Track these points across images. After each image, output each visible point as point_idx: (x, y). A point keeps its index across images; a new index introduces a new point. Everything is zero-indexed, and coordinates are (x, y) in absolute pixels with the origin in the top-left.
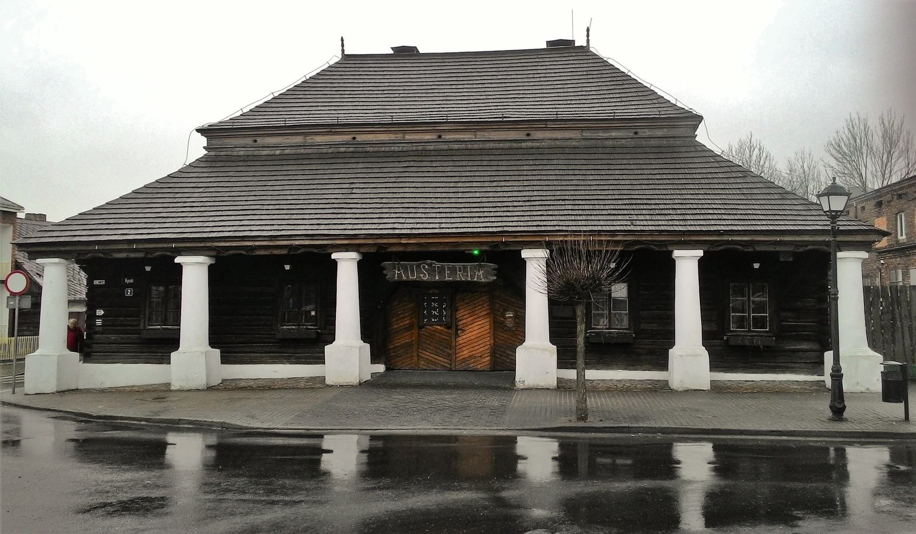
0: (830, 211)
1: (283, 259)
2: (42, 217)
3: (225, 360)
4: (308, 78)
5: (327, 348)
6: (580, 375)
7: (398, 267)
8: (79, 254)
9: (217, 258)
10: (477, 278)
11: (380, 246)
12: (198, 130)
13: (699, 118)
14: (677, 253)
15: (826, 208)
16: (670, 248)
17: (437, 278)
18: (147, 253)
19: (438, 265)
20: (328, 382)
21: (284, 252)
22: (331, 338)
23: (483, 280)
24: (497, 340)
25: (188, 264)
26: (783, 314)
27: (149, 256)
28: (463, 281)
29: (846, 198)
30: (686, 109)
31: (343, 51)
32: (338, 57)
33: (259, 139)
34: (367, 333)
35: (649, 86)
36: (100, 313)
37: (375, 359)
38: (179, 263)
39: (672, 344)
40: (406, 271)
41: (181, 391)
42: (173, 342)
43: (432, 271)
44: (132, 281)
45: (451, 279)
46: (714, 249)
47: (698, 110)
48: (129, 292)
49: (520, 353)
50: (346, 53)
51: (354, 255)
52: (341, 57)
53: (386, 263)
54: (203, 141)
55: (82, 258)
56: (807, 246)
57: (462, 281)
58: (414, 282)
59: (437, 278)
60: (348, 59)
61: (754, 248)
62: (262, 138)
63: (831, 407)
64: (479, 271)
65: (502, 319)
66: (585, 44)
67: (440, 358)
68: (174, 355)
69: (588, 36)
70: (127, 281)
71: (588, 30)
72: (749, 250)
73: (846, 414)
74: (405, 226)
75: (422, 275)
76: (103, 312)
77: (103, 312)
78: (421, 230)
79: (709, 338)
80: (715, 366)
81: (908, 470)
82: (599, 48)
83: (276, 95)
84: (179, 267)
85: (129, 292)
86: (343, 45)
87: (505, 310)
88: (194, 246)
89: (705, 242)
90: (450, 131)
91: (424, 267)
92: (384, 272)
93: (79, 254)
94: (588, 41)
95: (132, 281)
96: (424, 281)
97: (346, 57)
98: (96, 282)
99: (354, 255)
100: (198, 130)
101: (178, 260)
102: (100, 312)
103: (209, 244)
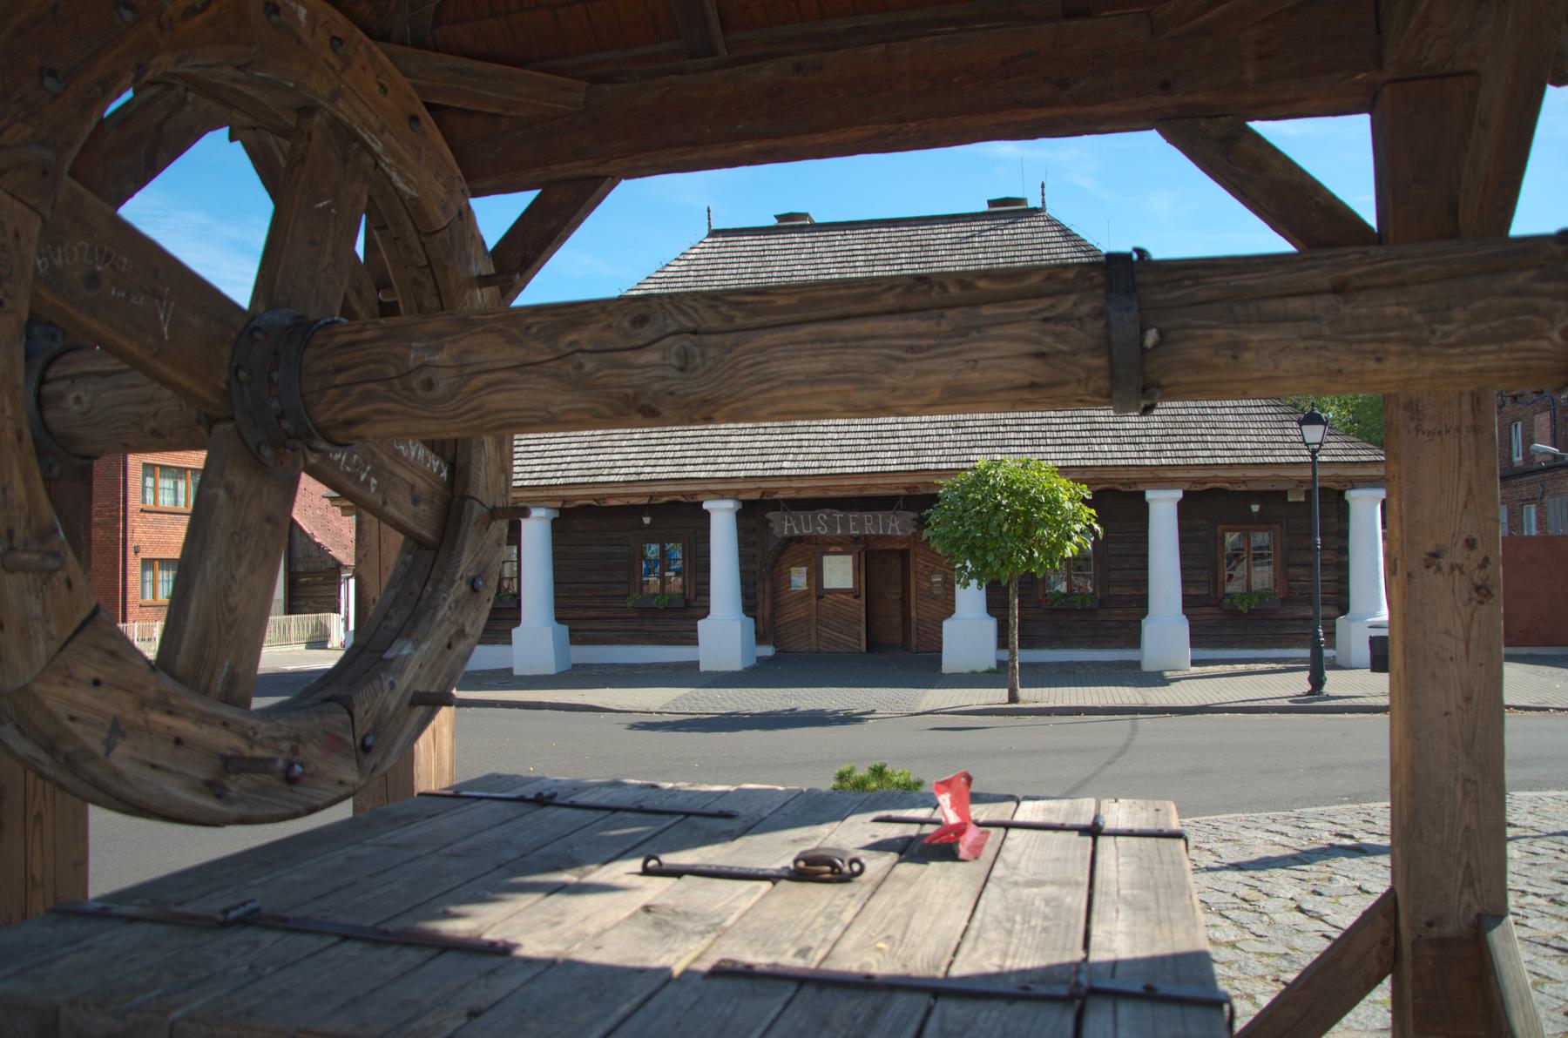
1: (639, 510)
3: (574, 641)
5: (701, 624)
7: (789, 519)
11: (765, 492)
14: (1150, 495)
17: (839, 532)
18: (564, 502)
19: (838, 515)
20: (516, 672)
22: (705, 611)
23: (899, 533)
24: (920, 612)
26: (1292, 571)
27: (653, 502)
31: (710, 226)
34: (749, 606)
37: (760, 639)
39: (1145, 613)
43: (831, 524)
45: (857, 532)
46: (1198, 489)
49: (948, 626)
56: (1205, 483)
57: (871, 535)
59: (839, 532)
65: (928, 585)
67: (845, 637)
74: (1074, 455)
75: (819, 528)
79: (1189, 603)
87: (933, 572)
88: (1160, 477)
89: (1185, 480)
91: (822, 517)
94: (1043, 202)
103: (551, 493)
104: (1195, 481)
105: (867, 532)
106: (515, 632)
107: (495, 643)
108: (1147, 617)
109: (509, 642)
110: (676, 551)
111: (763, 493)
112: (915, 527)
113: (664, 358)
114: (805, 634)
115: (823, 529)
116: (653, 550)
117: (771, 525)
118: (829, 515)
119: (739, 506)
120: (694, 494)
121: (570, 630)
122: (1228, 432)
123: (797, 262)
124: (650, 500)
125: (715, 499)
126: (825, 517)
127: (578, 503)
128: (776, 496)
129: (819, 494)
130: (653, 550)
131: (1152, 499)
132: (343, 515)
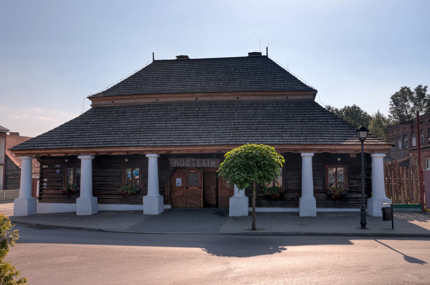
2: (17, 134)
3: (99, 202)
4: (137, 72)
5: (144, 198)
6: (254, 209)
7: (176, 161)
8: (37, 155)
9: (96, 156)
10: (212, 166)
14: (303, 154)
16: (299, 152)
17: (194, 165)
18: (66, 154)
19: (193, 160)
21: (125, 154)
23: (215, 166)
25: (84, 159)
27: (67, 155)
28: (205, 167)
29: (367, 132)
30: (310, 87)
31: (153, 58)
32: (151, 62)
33: (114, 101)
35: (294, 75)
36: (45, 180)
38: (80, 159)
40: (179, 162)
42: (77, 193)
43: (191, 163)
44: (59, 166)
45: (200, 166)
51: (155, 155)
52: (152, 61)
54: (90, 102)
55: (38, 156)
59: (194, 165)
60: (155, 62)
61: (336, 152)
63: (361, 223)
64: (213, 162)
65: (225, 184)
66: (266, 55)
68: (78, 200)
69: (267, 51)
70: (57, 166)
71: (267, 48)
72: (334, 153)
73: (367, 226)
75: (187, 164)
76: (47, 180)
77: (47, 180)
80: (318, 205)
83: (123, 80)
84: (80, 160)
85: (58, 171)
86: (153, 56)
90: (201, 96)
91: (188, 160)
92: (170, 163)
93: (37, 155)
94: (267, 53)
95: (59, 166)
96: (188, 167)
97: (155, 61)
98: (44, 167)
99: (155, 155)
100: (88, 98)
101: (79, 157)
102: (46, 180)
104: (318, 150)
105: (203, 166)
109: (75, 203)
115: (188, 165)
117: (170, 163)
118: (190, 160)
119: (159, 156)
120: (143, 151)
126: (189, 160)
128: (172, 153)
129: (187, 152)
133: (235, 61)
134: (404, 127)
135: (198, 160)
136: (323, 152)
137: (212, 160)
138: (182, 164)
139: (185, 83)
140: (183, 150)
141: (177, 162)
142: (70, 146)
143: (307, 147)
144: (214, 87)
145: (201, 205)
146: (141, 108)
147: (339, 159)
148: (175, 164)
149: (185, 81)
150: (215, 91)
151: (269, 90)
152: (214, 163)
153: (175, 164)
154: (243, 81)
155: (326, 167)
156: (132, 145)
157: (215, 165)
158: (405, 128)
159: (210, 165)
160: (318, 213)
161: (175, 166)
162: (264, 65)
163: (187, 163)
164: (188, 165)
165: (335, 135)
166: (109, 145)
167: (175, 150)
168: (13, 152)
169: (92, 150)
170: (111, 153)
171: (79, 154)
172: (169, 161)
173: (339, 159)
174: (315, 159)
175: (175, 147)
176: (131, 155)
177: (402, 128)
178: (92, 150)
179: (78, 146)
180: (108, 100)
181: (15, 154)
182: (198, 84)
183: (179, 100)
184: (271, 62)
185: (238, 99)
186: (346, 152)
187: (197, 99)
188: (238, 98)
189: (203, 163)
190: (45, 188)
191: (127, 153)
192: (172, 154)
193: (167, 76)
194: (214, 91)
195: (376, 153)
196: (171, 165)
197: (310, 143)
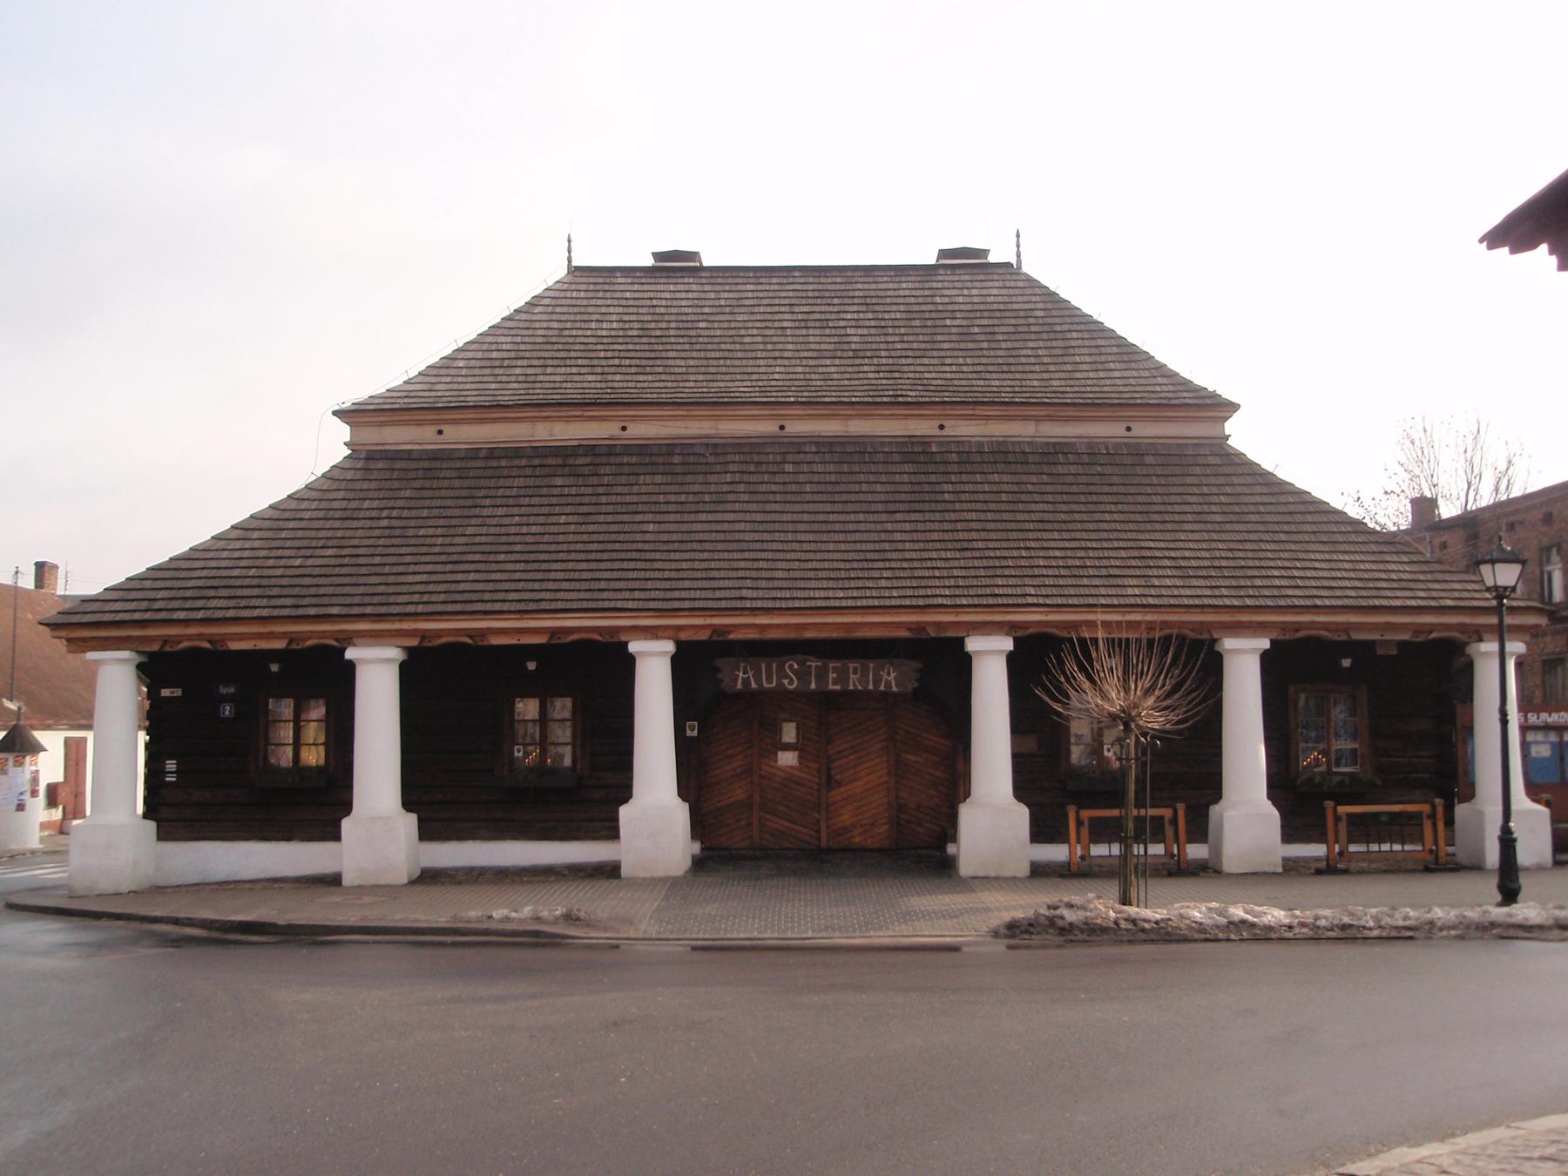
0: (1496, 588)
7: (745, 668)
10: (885, 686)
12: (335, 413)
13: (1232, 407)
14: (1229, 644)
15: (1490, 583)
16: (623, 639)
17: (813, 686)
18: (423, 638)
19: (813, 664)
22: (624, 792)
23: (895, 689)
28: (860, 691)
31: (570, 260)
32: (561, 272)
41: (353, 887)
43: (803, 675)
44: (232, 690)
45: (838, 687)
47: (1227, 394)
48: (227, 710)
50: (575, 263)
53: (720, 662)
54: (343, 431)
58: (771, 692)
59: (813, 686)
61: (1349, 635)
62: (456, 427)
64: (889, 674)
67: (798, 828)
70: (223, 690)
78: (626, 563)
81: (1344, 1165)
82: (1025, 269)
85: (227, 710)
89: (1274, 625)
90: (800, 417)
91: (791, 667)
92: (719, 676)
94: (1018, 255)
96: (791, 692)
98: (165, 693)
100: (335, 413)
104: (1284, 627)
105: (851, 688)
106: (346, 824)
107: (288, 839)
108: (1223, 803)
109: (336, 837)
110: (317, 711)
111: (714, 631)
112: (917, 680)
113: (1036, 431)
114: (743, 823)
115: (791, 682)
116: (528, 708)
117: (719, 676)
119: (137, 659)
121: (420, 820)
122: (1317, 565)
123: (701, 317)
124: (551, 638)
125: (645, 639)
126: (796, 666)
127: (444, 640)
128: (731, 636)
129: (792, 635)
130: (528, 708)
131: (976, 652)
132: (69, 652)
133: (897, 279)
134: (1437, 541)
135: (831, 665)
136: (1300, 634)
137: (888, 666)
138: (769, 680)
139: (722, 362)
140: (778, 625)
141: (750, 674)
142: (288, 610)
143: (1245, 618)
144: (842, 383)
145: (819, 840)
146: (560, 461)
147: (1346, 663)
148: (740, 682)
149: (721, 354)
150: (858, 400)
151: (1062, 401)
152: (893, 675)
153: (740, 682)
154: (949, 361)
155: (1291, 689)
156: (575, 605)
157: (896, 685)
158: (1444, 546)
159: (877, 682)
160: (1285, 860)
161: (739, 686)
162: (1014, 299)
163: (787, 676)
164: (791, 682)
165: (502, 557)
166: (479, 607)
167: (744, 626)
168: (63, 633)
169: (406, 626)
170: (483, 635)
171: (349, 639)
172: (719, 670)
173: (1346, 663)
174: (1015, 663)
175: (1199, 610)
176: (303, 650)
177: (1431, 542)
178: (406, 626)
179: (344, 611)
180: (420, 423)
181: (69, 640)
182: (778, 369)
183: (713, 432)
184: (1039, 287)
185: (945, 432)
186: (521, 642)
187: (782, 428)
188: (942, 427)
189: (852, 676)
190: (170, 779)
191: (161, 643)
192: (733, 642)
193: (641, 333)
194: (854, 400)
195: (1487, 641)
196: (724, 684)
197: (1139, 602)
